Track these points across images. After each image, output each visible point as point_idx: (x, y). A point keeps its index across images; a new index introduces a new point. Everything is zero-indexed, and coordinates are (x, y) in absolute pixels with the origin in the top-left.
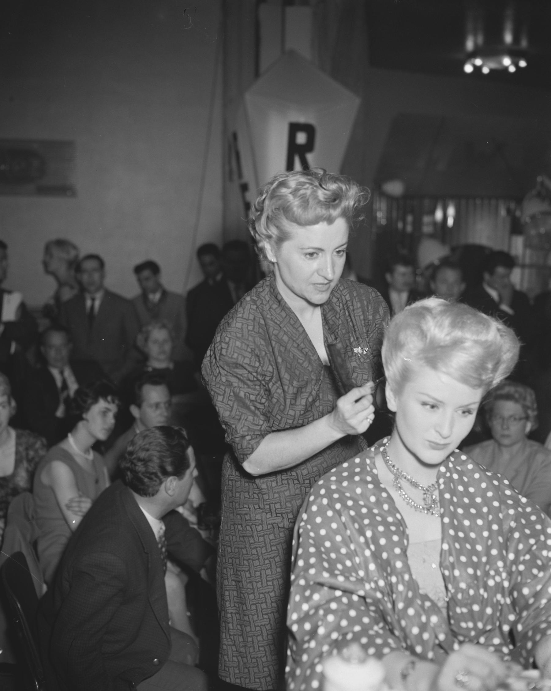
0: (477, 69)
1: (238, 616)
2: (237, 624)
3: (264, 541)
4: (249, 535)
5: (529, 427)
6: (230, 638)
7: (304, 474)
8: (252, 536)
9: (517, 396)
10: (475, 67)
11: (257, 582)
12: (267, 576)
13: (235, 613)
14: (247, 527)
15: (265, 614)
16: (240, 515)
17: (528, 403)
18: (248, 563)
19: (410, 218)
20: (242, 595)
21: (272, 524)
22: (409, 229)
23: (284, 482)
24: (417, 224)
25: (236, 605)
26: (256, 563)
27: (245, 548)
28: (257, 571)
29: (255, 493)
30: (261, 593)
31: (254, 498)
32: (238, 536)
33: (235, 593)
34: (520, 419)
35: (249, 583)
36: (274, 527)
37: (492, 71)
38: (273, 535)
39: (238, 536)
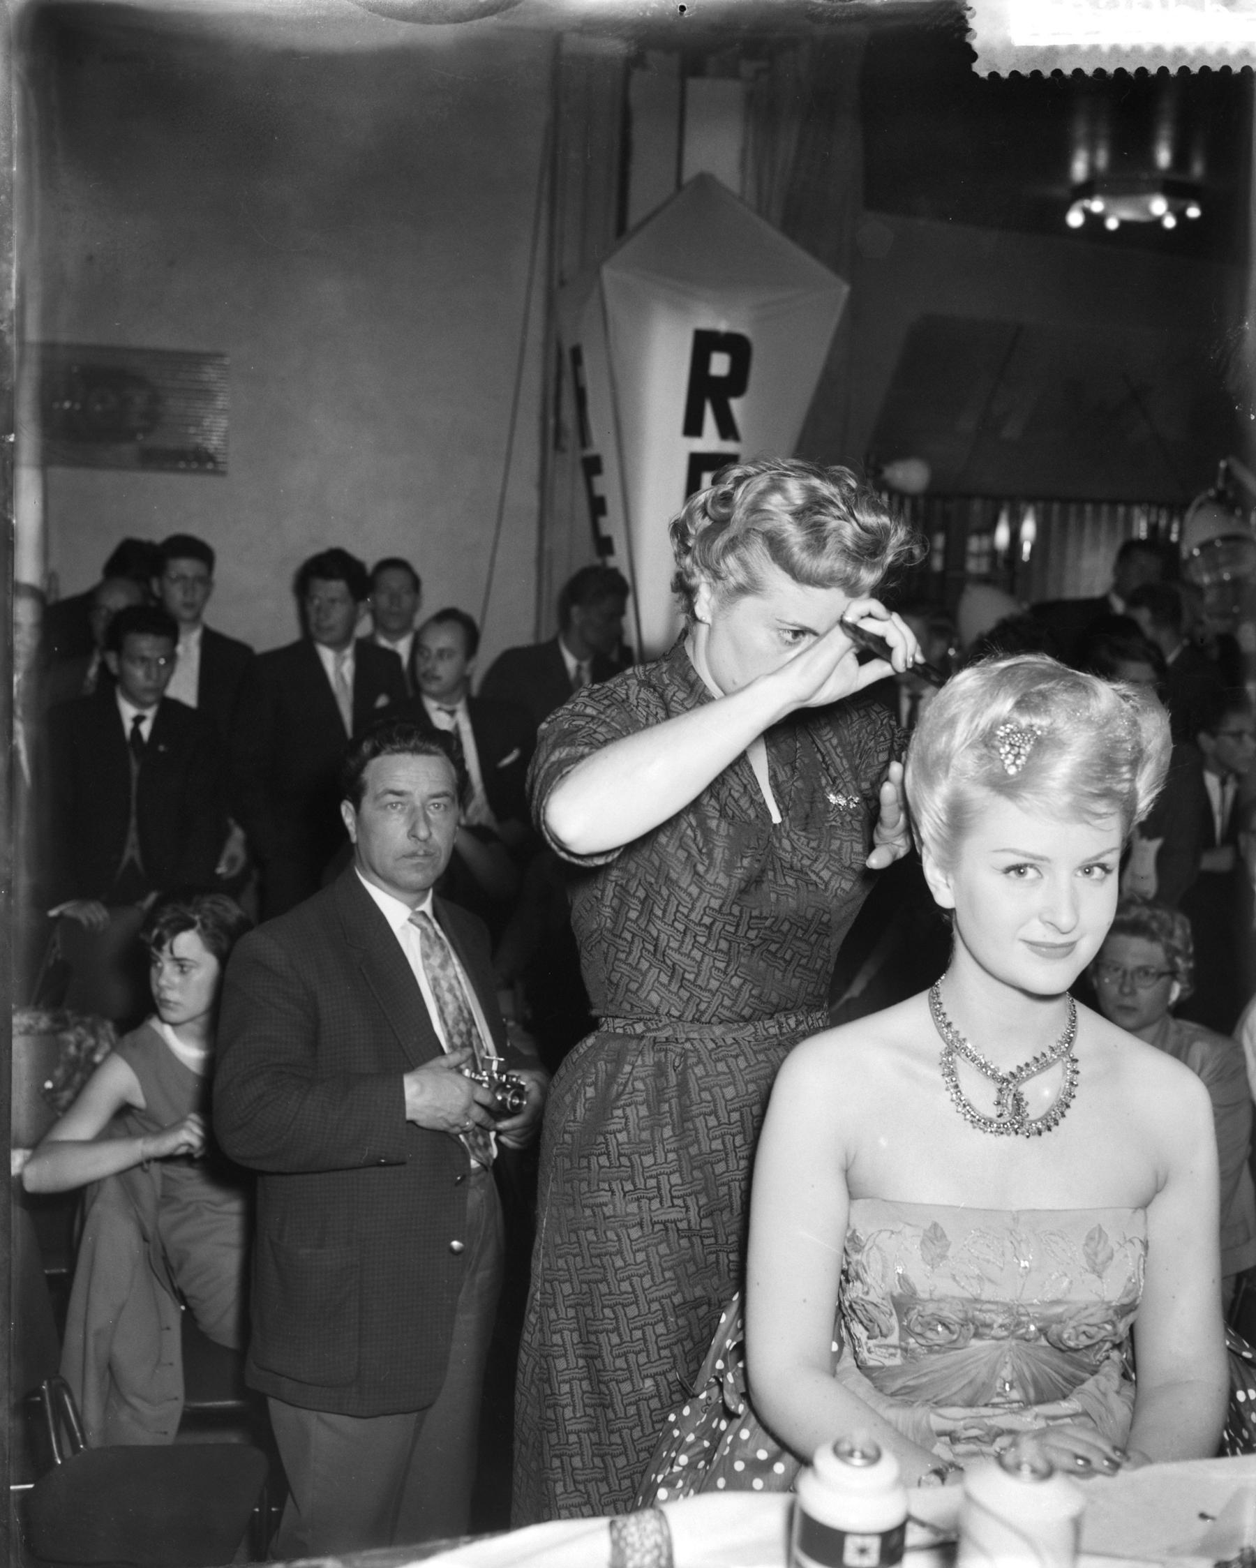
0: (1094, 221)
1: (594, 1437)
2: (594, 1455)
3: (648, 1260)
4: (614, 1250)
5: (1176, 992)
6: (577, 1490)
7: (728, 1097)
8: (620, 1252)
9: (1154, 925)
10: (1087, 213)
11: (637, 1353)
12: (657, 1337)
13: (587, 1432)
14: (609, 1233)
15: (664, 1348)
16: (591, 1207)
17: (1177, 943)
18: (614, 1312)
19: (939, 541)
20: (603, 1387)
21: (664, 1223)
22: (937, 563)
23: (676, 1202)
24: (956, 553)
25: (590, 1411)
26: (632, 1311)
27: (605, 1280)
28: (635, 1328)
29: (624, 1155)
30: (641, 1450)
31: (621, 1166)
32: (587, 1256)
33: (585, 1384)
34: (1160, 975)
35: (619, 1356)
36: (666, 1229)
37: (1124, 224)
38: (662, 1324)
39: (587, 1256)
